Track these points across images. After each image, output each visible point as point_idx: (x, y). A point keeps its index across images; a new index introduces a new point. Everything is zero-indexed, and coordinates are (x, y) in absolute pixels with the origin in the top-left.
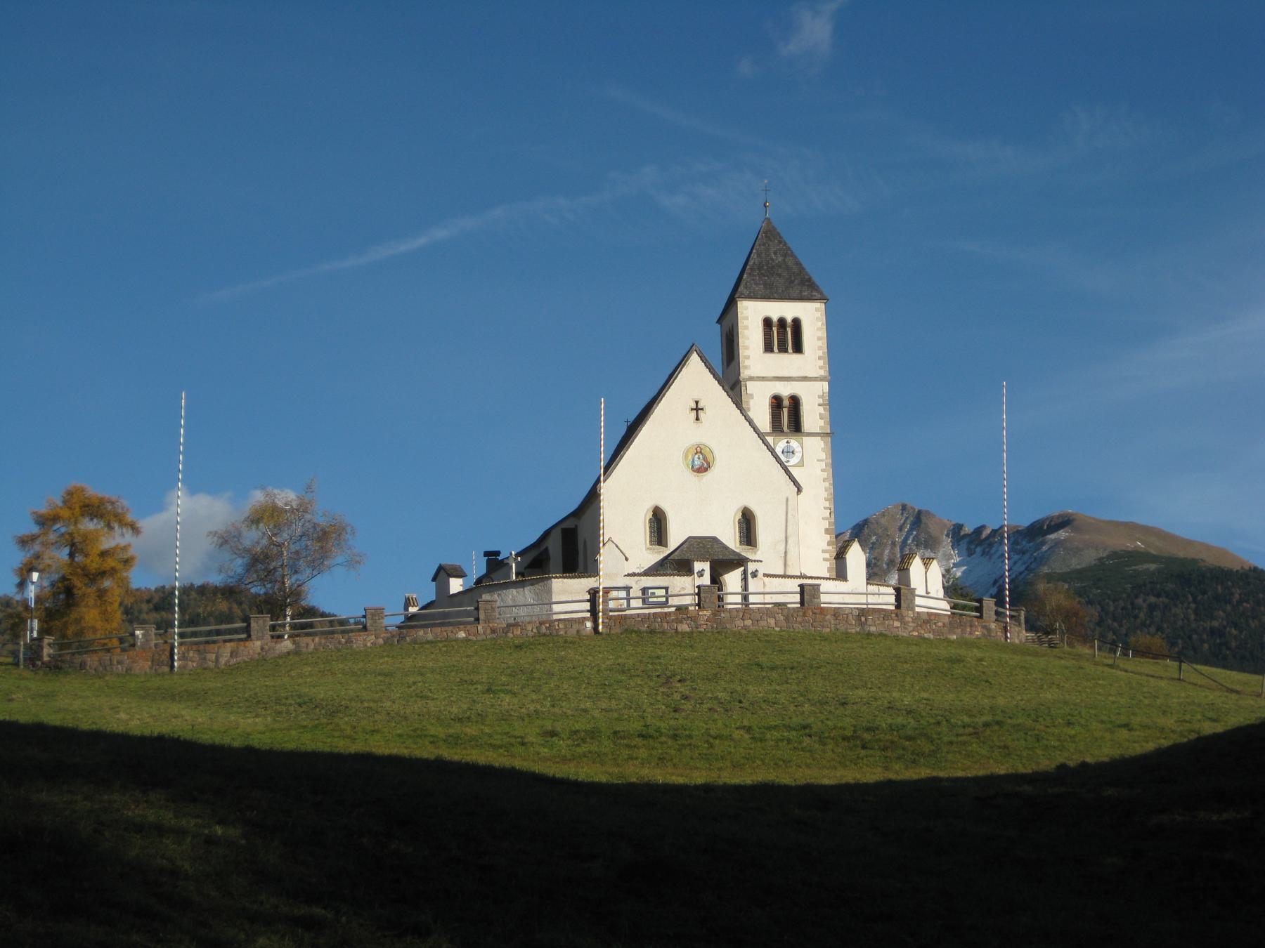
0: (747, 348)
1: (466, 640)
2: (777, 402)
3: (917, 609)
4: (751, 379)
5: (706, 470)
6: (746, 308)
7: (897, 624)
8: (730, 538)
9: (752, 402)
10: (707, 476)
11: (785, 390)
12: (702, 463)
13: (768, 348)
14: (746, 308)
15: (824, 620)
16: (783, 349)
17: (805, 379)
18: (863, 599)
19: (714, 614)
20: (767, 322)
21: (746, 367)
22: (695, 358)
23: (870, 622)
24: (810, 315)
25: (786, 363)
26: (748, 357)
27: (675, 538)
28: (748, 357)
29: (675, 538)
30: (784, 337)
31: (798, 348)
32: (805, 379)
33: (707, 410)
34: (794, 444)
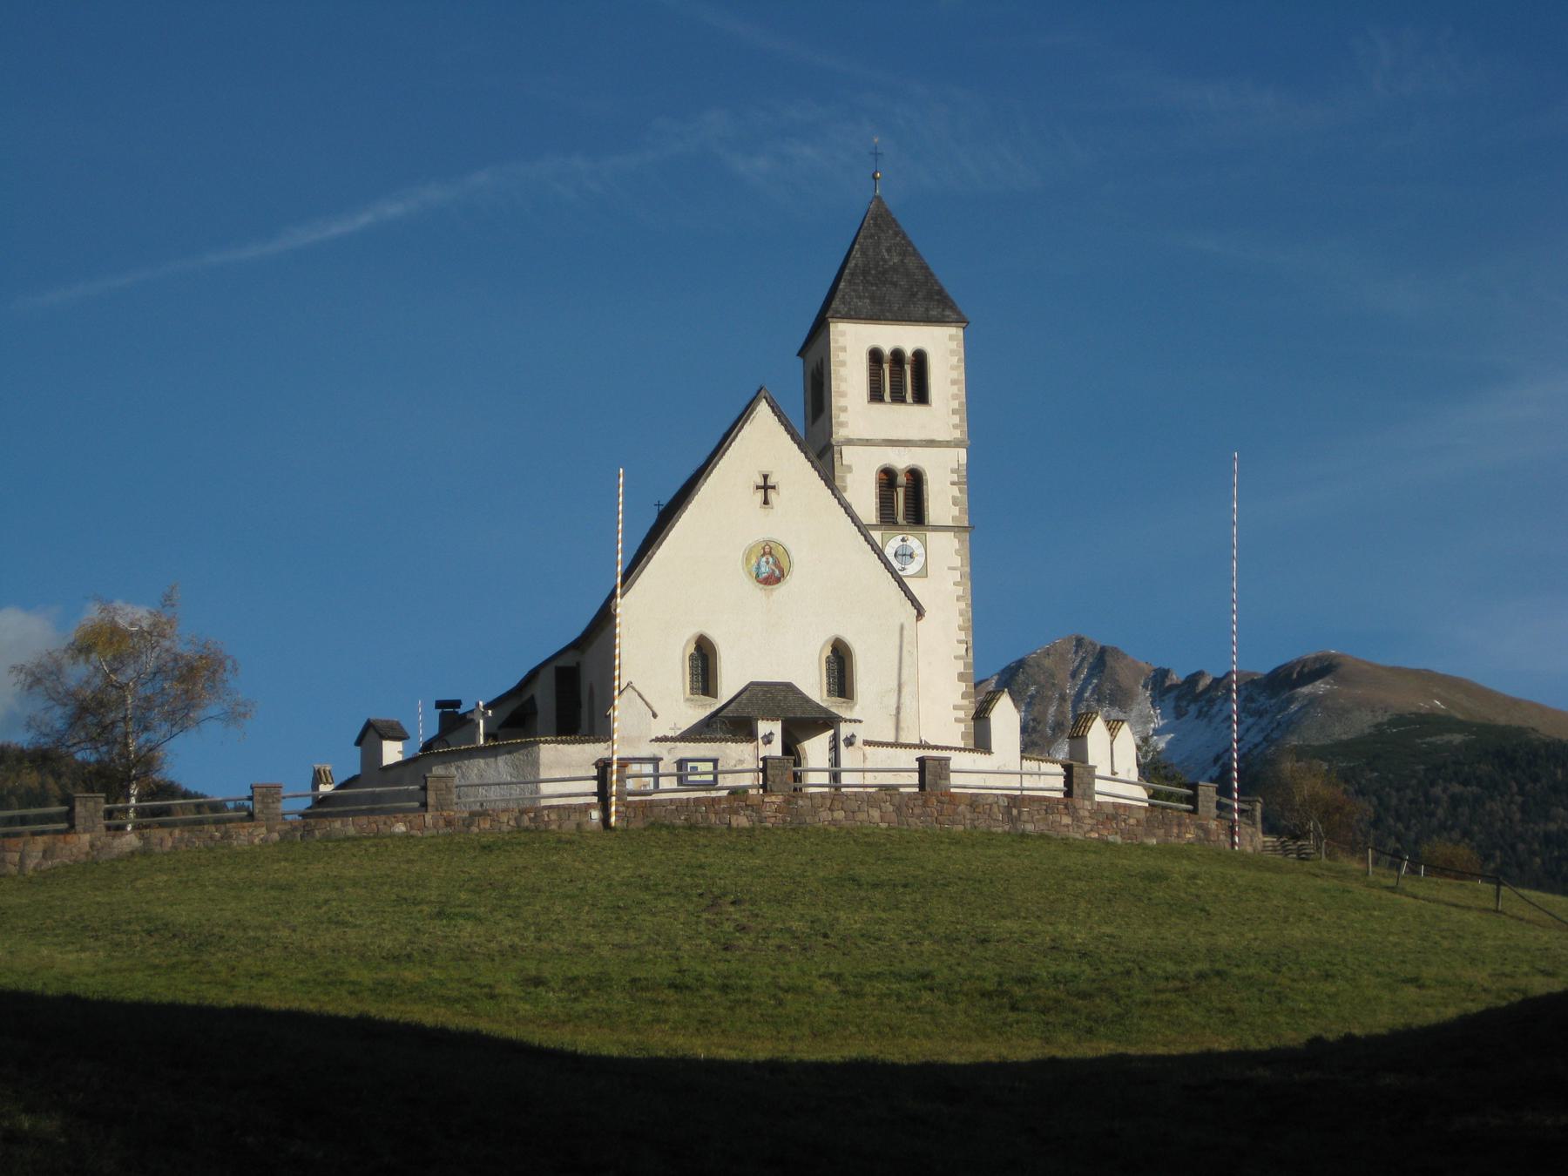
0: (843, 395)
1: (407, 837)
2: (888, 478)
3: (1098, 798)
4: (850, 442)
5: (778, 580)
6: (843, 334)
7: (1066, 820)
8: (814, 686)
9: (849, 478)
10: (780, 590)
11: (901, 460)
12: (771, 570)
13: (876, 395)
14: (843, 334)
15: (955, 812)
16: (898, 398)
17: (931, 443)
18: (1014, 781)
19: (787, 802)
20: (875, 356)
21: (842, 425)
22: (763, 409)
23: (1025, 817)
24: (940, 345)
25: (902, 419)
26: (844, 409)
27: (730, 684)
28: (844, 409)
29: (730, 684)
30: (901, 379)
31: (922, 397)
32: (931, 443)
33: (782, 489)
34: (913, 543)
